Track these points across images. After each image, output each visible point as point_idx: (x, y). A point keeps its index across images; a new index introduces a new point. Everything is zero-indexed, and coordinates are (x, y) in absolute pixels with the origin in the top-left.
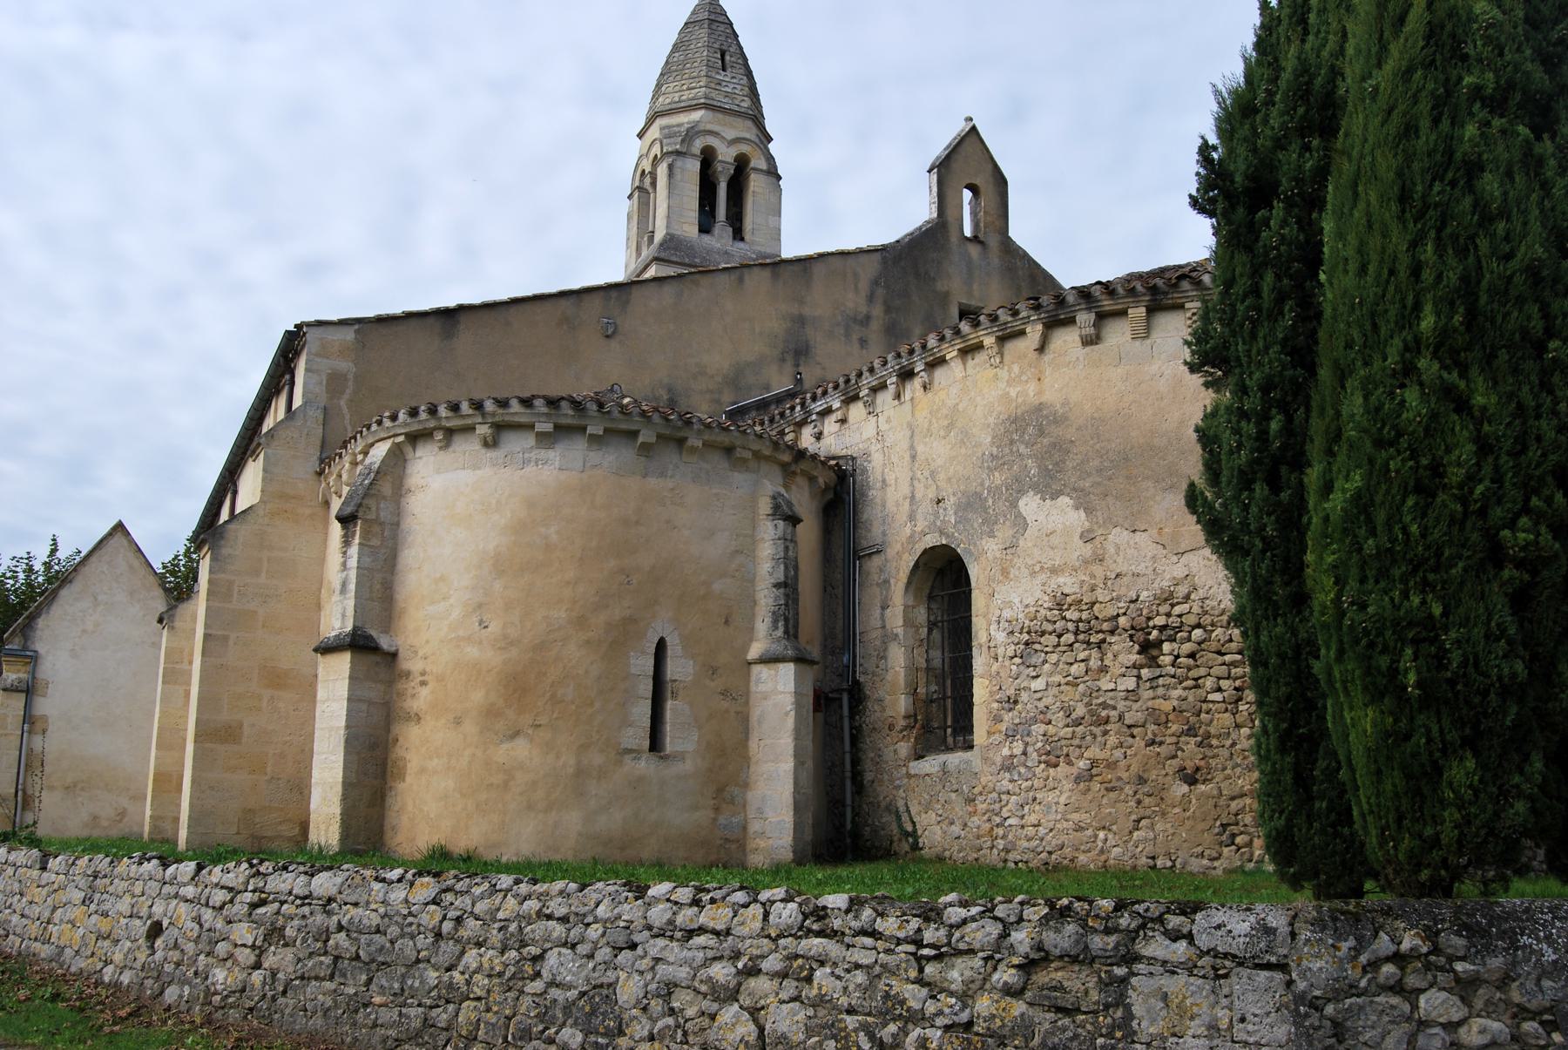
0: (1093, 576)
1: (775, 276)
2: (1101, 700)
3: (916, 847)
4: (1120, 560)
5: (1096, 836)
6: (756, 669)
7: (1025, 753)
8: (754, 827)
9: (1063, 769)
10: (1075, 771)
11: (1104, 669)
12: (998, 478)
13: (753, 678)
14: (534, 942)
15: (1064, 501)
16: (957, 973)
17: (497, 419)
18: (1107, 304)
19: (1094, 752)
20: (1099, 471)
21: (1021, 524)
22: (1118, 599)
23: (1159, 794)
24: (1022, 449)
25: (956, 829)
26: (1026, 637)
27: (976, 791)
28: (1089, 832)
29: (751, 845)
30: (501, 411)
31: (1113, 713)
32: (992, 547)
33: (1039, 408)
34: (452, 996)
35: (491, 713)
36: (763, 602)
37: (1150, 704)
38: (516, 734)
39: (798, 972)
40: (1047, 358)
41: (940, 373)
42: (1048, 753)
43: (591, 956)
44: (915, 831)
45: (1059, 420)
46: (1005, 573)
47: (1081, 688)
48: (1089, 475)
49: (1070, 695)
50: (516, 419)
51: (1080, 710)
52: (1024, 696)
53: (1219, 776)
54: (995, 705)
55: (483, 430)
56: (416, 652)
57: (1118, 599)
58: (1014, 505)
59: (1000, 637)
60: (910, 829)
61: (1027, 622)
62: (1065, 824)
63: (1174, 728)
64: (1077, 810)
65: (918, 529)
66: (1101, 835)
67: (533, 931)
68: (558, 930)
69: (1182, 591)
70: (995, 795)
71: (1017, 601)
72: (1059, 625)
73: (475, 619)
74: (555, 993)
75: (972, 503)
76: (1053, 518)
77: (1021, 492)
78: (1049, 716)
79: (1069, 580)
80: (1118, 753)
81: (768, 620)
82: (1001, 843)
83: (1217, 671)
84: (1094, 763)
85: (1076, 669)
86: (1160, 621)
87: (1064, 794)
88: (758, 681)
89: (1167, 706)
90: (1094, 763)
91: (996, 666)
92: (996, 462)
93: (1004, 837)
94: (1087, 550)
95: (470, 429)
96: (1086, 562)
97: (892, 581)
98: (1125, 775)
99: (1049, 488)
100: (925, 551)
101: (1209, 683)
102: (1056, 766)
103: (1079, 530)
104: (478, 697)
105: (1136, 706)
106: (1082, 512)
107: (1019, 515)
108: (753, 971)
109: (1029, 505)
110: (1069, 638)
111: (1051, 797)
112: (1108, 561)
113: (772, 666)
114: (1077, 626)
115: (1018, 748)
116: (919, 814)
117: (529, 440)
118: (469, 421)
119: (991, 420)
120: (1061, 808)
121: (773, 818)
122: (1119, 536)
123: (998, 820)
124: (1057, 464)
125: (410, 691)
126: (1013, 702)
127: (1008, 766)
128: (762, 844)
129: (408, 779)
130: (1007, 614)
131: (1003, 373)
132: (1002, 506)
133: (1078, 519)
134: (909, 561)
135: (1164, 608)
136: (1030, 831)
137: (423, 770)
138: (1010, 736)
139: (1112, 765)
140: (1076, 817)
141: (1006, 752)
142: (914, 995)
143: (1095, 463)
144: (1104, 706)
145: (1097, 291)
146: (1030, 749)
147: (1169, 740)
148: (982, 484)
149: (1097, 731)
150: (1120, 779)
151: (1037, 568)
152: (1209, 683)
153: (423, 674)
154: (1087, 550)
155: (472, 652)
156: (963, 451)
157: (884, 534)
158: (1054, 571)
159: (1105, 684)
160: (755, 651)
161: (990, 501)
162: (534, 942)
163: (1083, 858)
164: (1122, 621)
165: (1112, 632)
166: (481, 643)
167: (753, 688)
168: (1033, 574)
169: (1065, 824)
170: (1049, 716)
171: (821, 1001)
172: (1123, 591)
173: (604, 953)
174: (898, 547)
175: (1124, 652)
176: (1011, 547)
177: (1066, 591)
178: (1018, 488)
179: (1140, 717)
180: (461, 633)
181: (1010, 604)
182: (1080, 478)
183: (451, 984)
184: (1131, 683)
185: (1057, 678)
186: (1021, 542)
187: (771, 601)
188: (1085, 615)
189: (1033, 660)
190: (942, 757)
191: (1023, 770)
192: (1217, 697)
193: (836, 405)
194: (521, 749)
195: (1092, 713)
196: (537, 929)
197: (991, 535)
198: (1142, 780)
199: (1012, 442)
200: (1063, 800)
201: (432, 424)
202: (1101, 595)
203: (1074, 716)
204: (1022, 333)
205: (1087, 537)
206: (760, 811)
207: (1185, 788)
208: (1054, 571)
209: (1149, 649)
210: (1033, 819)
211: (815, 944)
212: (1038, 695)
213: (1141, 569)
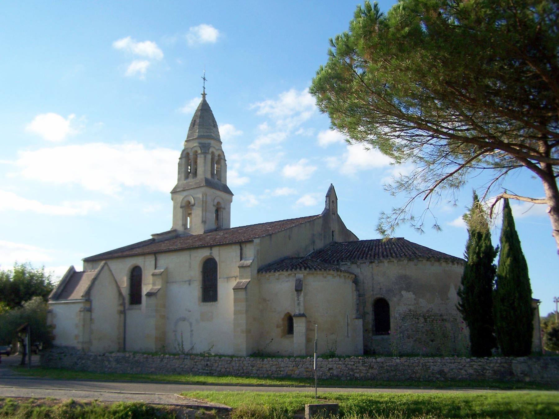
9: (411, 339)
11: (418, 322)
12: (397, 287)
15: (411, 293)
16: (492, 365)
21: (402, 296)
38: (332, 334)
39: (471, 366)
52: (403, 327)
58: (400, 292)
59: (397, 315)
65: (375, 293)
76: (408, 296)
85: (413, 322)
99: (408, 290)
108: (465, 366)
109: (403, 293)
111: (409, 344)
114: (412, 315)
115: (401, 335)
122: (421, 300)
126: (400, 327)
130: (399, 312)
139: (420, 339)
142: (487, 368)
158: (409, 305)
171: (475, 369)
173: (441, 366)
175: (422, 320)
184: (423, 325)
190: (382, 336)
193: (349, 264)
196: (429, 364)
197: (395, 297)
205: (415, 299)
208: (409, 305)
209: (425, 319)
211: (473, 363)
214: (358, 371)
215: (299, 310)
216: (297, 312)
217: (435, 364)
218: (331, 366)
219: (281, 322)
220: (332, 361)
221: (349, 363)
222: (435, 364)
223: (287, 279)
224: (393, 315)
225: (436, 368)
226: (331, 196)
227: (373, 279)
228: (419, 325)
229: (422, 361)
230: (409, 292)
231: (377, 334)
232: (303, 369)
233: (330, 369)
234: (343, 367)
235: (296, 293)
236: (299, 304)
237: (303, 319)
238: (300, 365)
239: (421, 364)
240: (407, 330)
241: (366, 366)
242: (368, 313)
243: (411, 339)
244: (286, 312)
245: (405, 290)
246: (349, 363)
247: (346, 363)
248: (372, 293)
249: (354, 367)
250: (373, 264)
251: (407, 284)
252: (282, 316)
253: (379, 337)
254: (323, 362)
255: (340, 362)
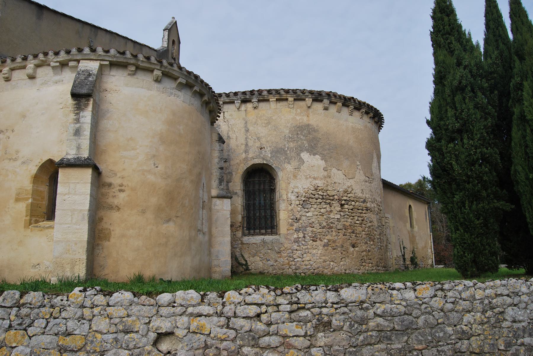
0: (327, 182)
1: (134, 46)
2: (331, 221)
3: (247, 269)
4: (335, 178)
5: (330, 264)
6: (214, 200)
7: (304, 237)
8: (215, 263)
9: (319, 242)
10: (323, 243)
11: (331, 211)
12: (292, 145)
13: (213, 203)
14: (498, 306)
15: (317, 156)
17: (167, 70)
18: (333, 99)
19: (329, 237)
20: (329, 149)
21: (302, 161)
22: (335, 190)
23: (347, 250)
24: (302, 137)
25: (271, 263)
26: (304, 199)
27: (281, 249)
28: (328, 262)
29: (214, 270)
30: (169, 67)
31: (334, 225)
32: (289, 168)
33: (308, 125)
34: (465, 336)
35: (159, 210)
36: (215, 174)
37: (343, 223)
38: (168, 221)
40: (310, 110)
41: (262, 105)
42: (313, 237)
43: (526, 308)
44: (247, 263)
45: (315, 131)
46: (295, 176)
47: (325, 216)
48: (326, 150)
49: (321, 219)
50: (174, 73)
51: (325, 224)
52: (304, 218)
53: (359, 245)
54: (291, 220)
55: (158, 73)
56: (116, 175)
57: (335, 190)
58: (299, 155)
59: (293, 197)
60: (244, 263)
61: (304, 194)
62: (320, 260)
63: (350, 231)
64: (324, 256)
65: (250, 156)
66: (332, 263)
67: (497, 302)
68: (509, 300)
69: (350, 190)
70: (290, 251)
71: (300, 186)
72: (317, 196)
73: (152, 162)
74: (516, 325)
75: (278, 151)
76: (313, 162)
77: (302, 151)
78: (313, 225)
79: (319, 182)
80: (336, 238)
81: (217, 181)
82: (294, 267)
83: (358, 214)
84: (329, 240)
86: (345, 198)
87: (320, 251)
88: (215, 205)
89: (348, 224)
90: (329, 240)
91: (290, 208)
92: (291, 139)
93: (295, 265)
94: (325, 173)
95: (152, 71)
96: (325, 177)
97: (234, 173)
98: (338, 245)
99: (312, 150)
100: (254, 165)
101: (356, 218)
102: (316, 241)
103: (323, 167)
104: (154, 200)
105: (340, 223)
106: (323, 161)
107: (301, 158)
109: (305, 155)
110: (319, 200)
111: (314, 251)
112: (332, 178)
113: (221, 199)
114: (320, 197)
116: (249, 257)
117: (174, 85)
118: (153, 67)
119: (289, 125)
120: (319, 255)
121: (223, 259)
122: (334, 170)
123: (292, 259)
124: (315, 144)
125: (111, 194)
126: (297, 220)
127: (297, 241)
128: (218, 269)
129: (112, 240)
130: (296, 190)
131: (294, 111)
132: (293, 154)
133: (322, 163)
134: (242, 168)
135: (346, 194)
136: (307, 263)
137: (123, 236)
138: (297, 230)
139: (334, 242)
140: (324, 258)
141: (295, 236)
143: (328, 147)
144: (332, 223)
145: (282, 92)
146: (306, 236)
147: (348, 234)
148: (285, 145)
149: (330, 230)
150: (337, 246)
151: (308, 177)
152: (356, 218)
153: (121, 185)
154: (325, 173)
155: (151, 178)
156: (275, 133)
157: (228, 155)
158: (315, 178)
159: (332, 216)
160: (214, 193)
161: (289, 152)
162: (498, 306)
163: (326, 271)
164: (336, 197)
165: (333, 200)
166: (155, 174)
167: (213, 207)
168: (307, 178)
169: (320, 260)
170: (313, 225)
172: (336, 188)
174: (238, 161)
176: (298, 168)
177: (319, 185)
178: (301, 149)
179: (341, 227)
180: (145, 168)
181: (297, 187)
182: (323, 150)
183: (463, 331)
184: (338, 216)
185: (316, 213)
186: (302, 167)
187: (218, 174)
188: (325, 194)
189: (307, 207)
191: (303, 242)
192: (357, 222)
194: (171, 227)
195: (328, 225)
196: (498, 301)
197: (289, 163)
198: (342, 246)
199: (298, 134)
200: (319, 252)
201: (132, 61)
202: (329, 188)
203: (322, 225)
204: (304, 100)
205: (325, 169)
206: (217, 256)
207: (353, 249)
208: (315, 178)
210: (308, 258)
212: (309, 218)
213: (340, 182)
214: (274, 341)
215: (79, 148)
216: (71, 154)
217: (516, 300)
218: (165, 326)
219: (28, 185)
220: (172, 304)
221: (240, 310)
222: (516, 300)
223: (57, 78)
224: (285, 197)
225: (520, 315)
226: (172, 30)
227: (247, 131)
228: (332, 216)
229: (479, 294)
230: (314, 154)
231: (249, 234)
232: (46, 339)
233: (161, 336)
234: (212, 326)
235: (70, 101)
236: (77, 133)
237: (88, 173)
238: (41, 323)
239: (477, 303)
240: (311, 225)
241: (305, 321)
242: (236, 193)
243: (319, 242)
244: (45, 159)
245: (307, 151)
246: (241, 310)
247: (228, 310)
248: (244, 155)
249: (260, 326)
250: (249, 106)
251: (309, 140)
252: (34, 169)
253: (257, 239)
254: (135, 309)
255: (205, 309)
